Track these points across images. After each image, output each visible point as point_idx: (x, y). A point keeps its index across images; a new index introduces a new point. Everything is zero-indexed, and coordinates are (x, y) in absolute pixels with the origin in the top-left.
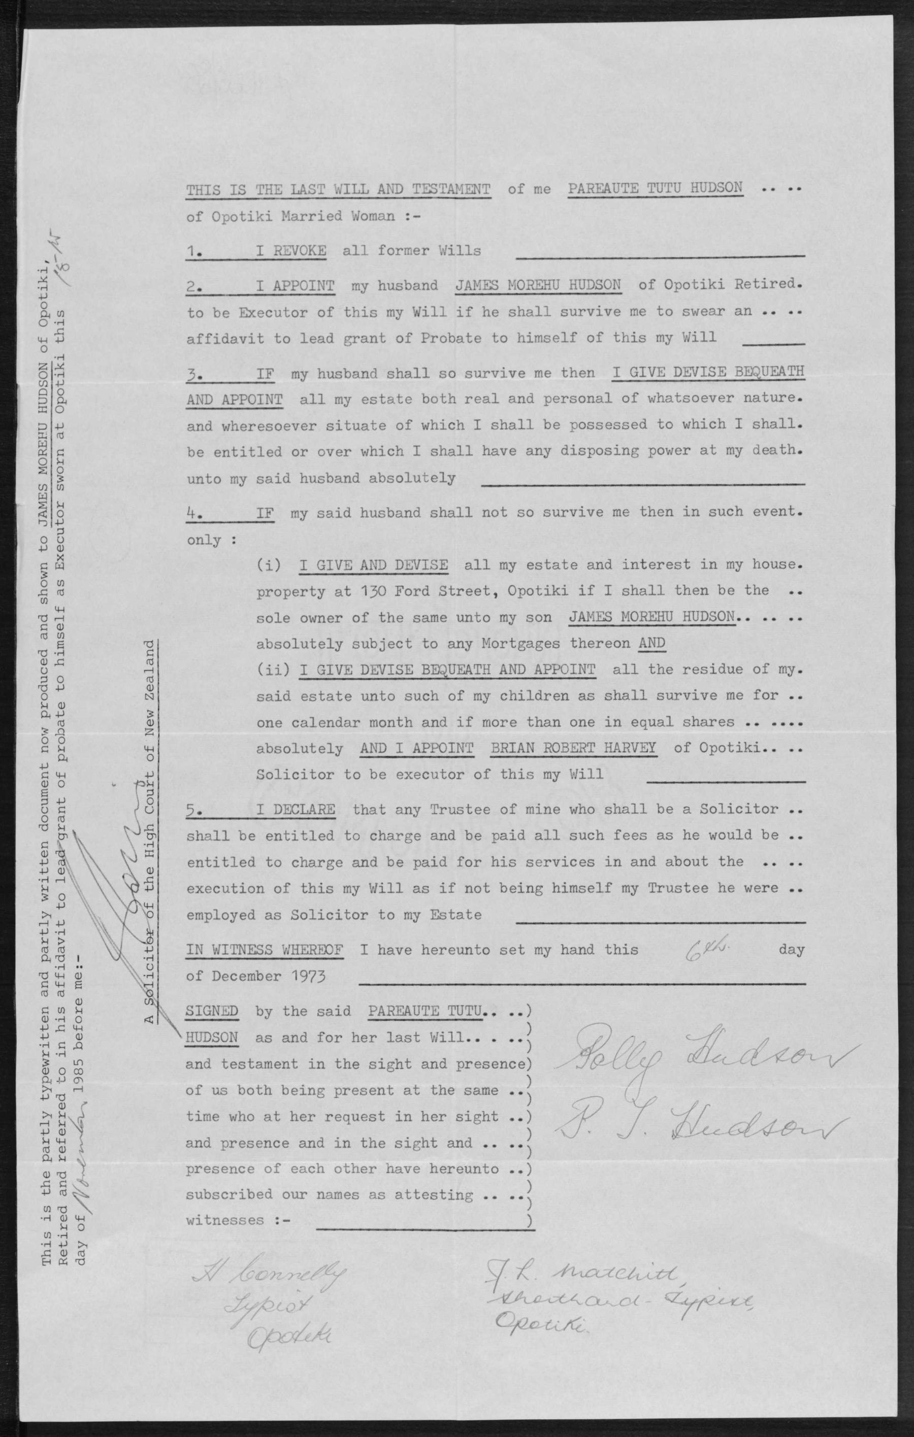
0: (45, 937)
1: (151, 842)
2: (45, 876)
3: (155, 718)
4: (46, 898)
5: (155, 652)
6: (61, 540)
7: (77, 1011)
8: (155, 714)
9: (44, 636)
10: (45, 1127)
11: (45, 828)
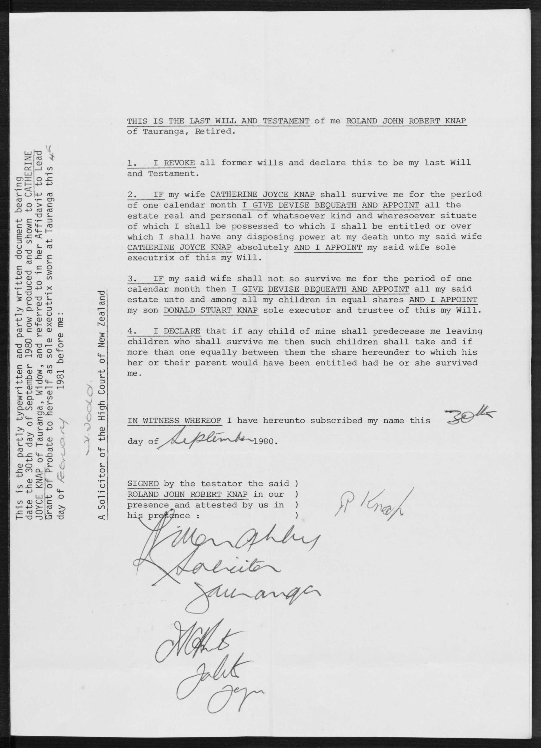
7: (234, 162)
9: (250, 332)
11: (365, 237)
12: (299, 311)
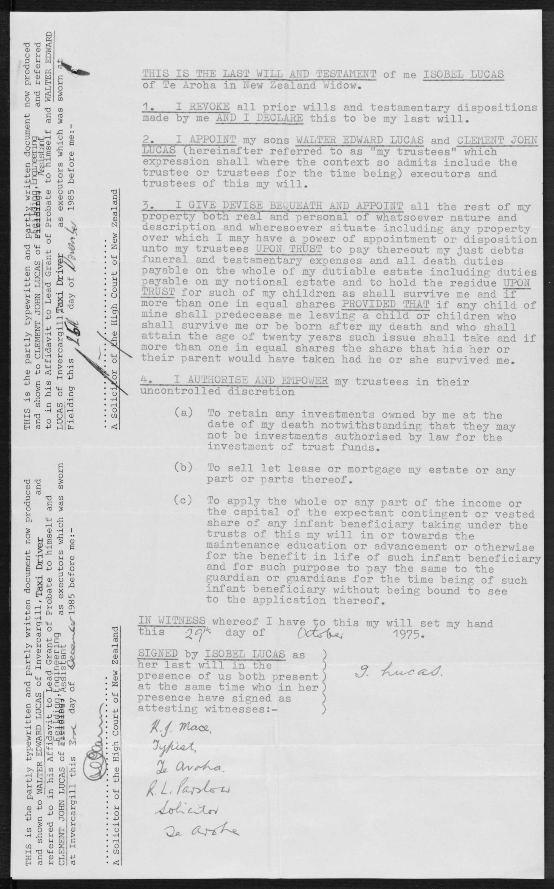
0: (30, 784)
1: (115, 316)
2: (28, 725)
3: (118, 238)
4: (29, 635)
5: (119, 635)
6: (61, 580)
10: (28, 653)
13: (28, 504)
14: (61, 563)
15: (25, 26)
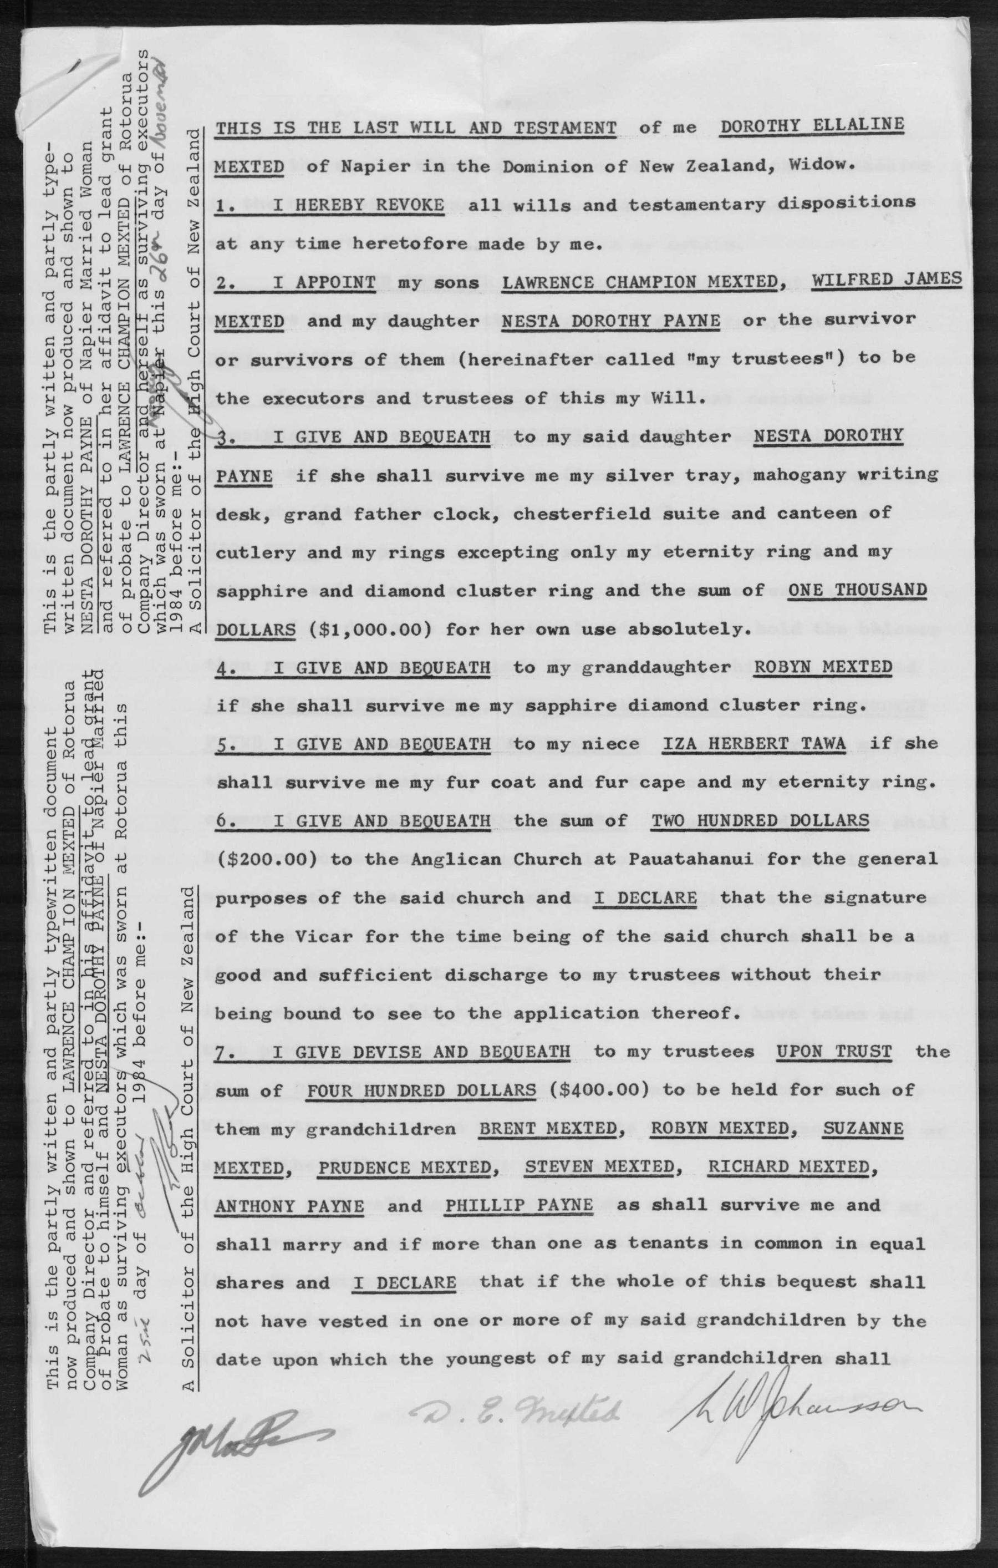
0: (51, 463)
1: (189, 1153)
2: (51, 1140)
3: (194, 989)
8: (195, 984)
12: (121, 1152)
13: (68, 353)
14: (127, 112)
15: (70, 75)
